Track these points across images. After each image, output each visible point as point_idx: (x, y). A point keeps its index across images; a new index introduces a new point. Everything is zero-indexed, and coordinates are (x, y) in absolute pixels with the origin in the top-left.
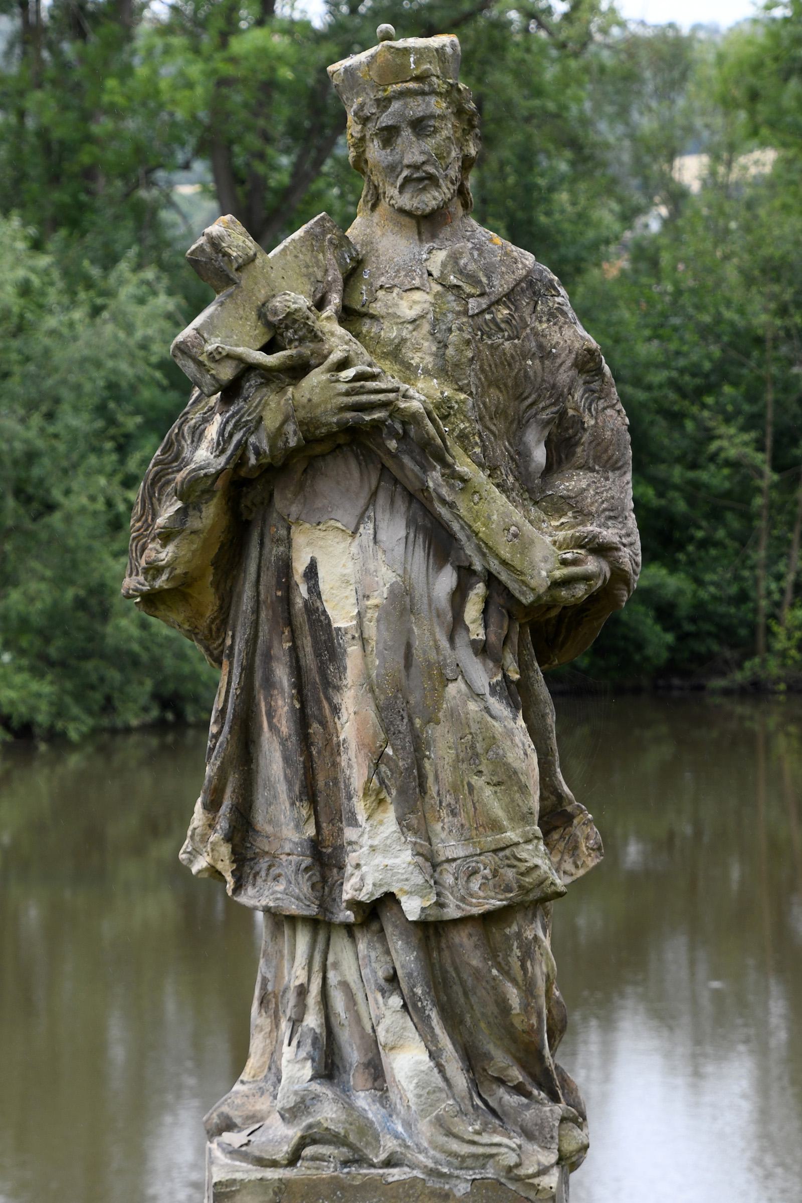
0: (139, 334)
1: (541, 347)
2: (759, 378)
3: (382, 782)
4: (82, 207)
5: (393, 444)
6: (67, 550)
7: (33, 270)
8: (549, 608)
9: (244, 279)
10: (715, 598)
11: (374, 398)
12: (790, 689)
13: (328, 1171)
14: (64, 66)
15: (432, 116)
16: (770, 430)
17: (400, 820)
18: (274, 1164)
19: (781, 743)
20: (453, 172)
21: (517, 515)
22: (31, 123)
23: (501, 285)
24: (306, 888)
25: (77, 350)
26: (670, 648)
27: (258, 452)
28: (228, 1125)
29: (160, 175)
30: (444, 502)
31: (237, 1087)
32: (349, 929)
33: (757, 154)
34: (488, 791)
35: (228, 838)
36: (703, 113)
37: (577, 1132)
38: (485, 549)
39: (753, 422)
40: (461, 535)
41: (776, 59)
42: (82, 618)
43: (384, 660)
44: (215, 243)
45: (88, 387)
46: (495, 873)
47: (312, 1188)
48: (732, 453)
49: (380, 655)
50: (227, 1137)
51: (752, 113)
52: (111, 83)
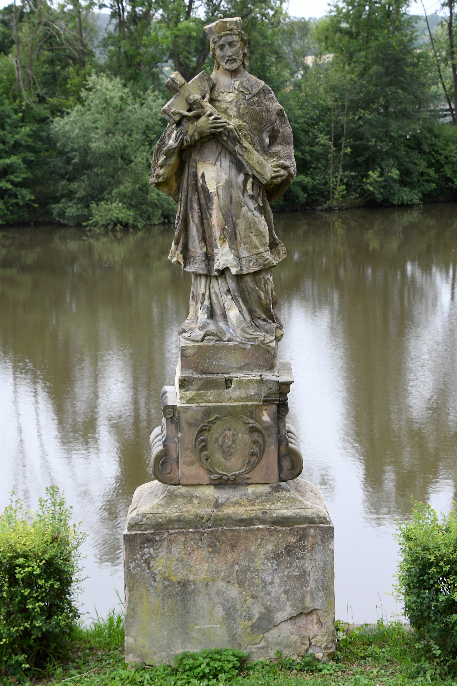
0: (154, 111)
1: (267, 109)
2: (330, 120)
3: (224, 236)
4: (137, 74)
5: (225, 138)
6: (136, 174)
7: (124, 93)
8: (271, 185)
9: (182, 90)
10: (318, 184)
11: (219, 125)
12: (339, 209)
13: (212, 343)
14: (131, 33)
15: (234, 41)
16: (333, 135)
17: (230, 246)
18: (197, 341)
19: (337, 224)
20: (241, 58)
21: (261, 158)
22: (122, 50)
23: (255, 91)
24: (204, 266)
25: (136, 116)
26: (306, 198)
27: (187, 141)
28: (185, 331)
29: (159, 64)
30: (240, 155)
31: (186, 321)
32: (216, 277)
33: (328, 55)
34: (254, 238)
35: (182, 253)
36: (313, 43)
37: (280, 331)
38: (252, 168)
39: (328, 133)
40: (245, 164)
41: (333, 27)
42: (141, 193)
43: (224, 201)
44: (173, 80)
45: (140, 126)
46: (257, 261)
47: (208, 348)
48: (323, 142)
49: (223, 199)
50: (184, 334)
51: (326, 43)
52: (145, 38)
